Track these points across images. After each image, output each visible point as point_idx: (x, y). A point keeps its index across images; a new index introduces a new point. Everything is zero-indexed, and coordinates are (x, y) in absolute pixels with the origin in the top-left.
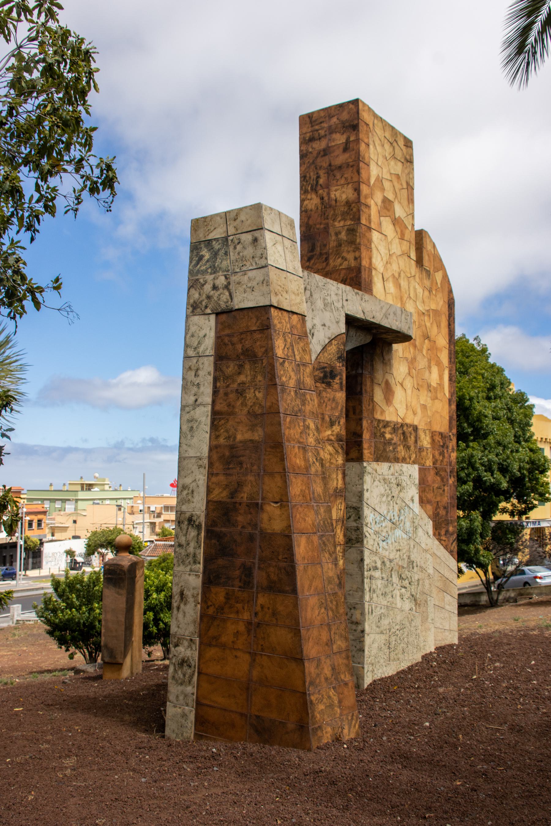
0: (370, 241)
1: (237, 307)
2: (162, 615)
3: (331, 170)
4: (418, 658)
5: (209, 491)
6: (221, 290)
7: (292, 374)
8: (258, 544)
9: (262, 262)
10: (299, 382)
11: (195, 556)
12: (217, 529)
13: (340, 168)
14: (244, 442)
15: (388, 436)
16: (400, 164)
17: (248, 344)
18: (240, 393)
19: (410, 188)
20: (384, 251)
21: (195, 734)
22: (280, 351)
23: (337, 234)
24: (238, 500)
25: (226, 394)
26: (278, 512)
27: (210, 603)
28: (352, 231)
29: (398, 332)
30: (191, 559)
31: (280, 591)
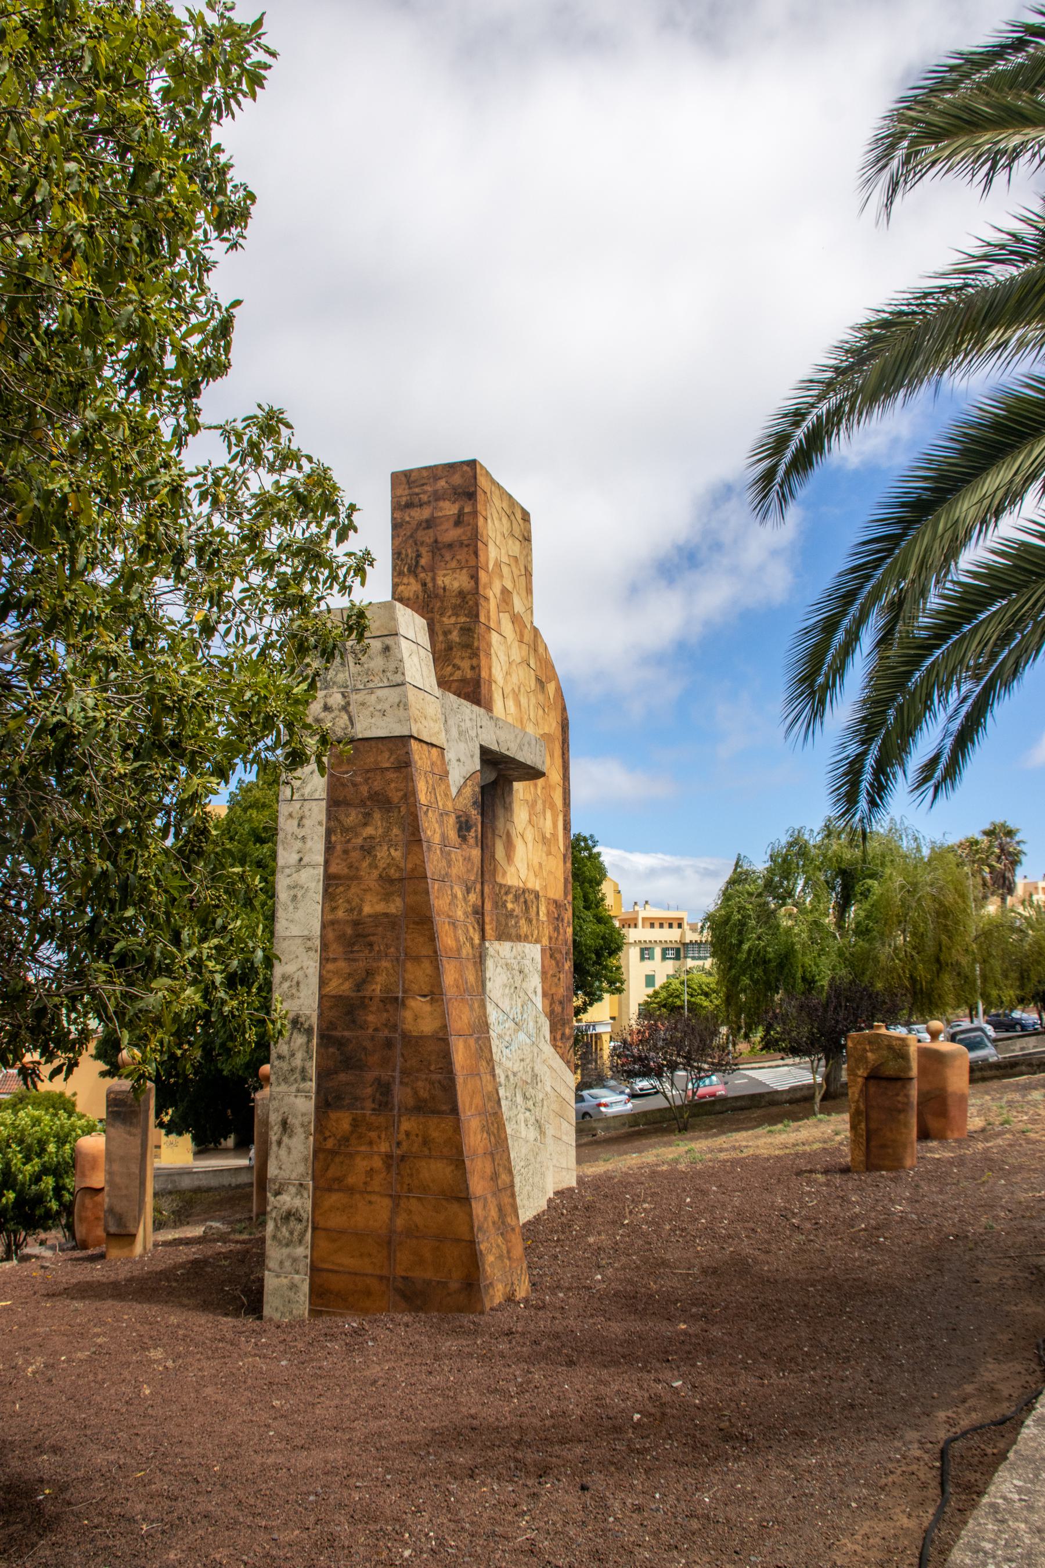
0: (489, 645)
1: (360, 736)
2: (67, 1181)
3: (437, 548)
4: (543, 1205)
5: (323, 982)
6: (336, 713)
7: (436, 826)
8: (398, 1052)
9: (398, 678)
10: (444, 837)
11: (303, 1070)
12: (337, 1034)
13: (450, 546)
14: (375, 916)
15: (510, 906)
16: (518, 543)
17: (377, 785)
18: (368, 850)
19: (528, 574)
20: (503, 660)
21: (310, 1311)
22: (423, 798)
23: (446, 633)
24: (367, 994)
25: (346, 852)
26: (427, 1008)
27: (327, 1134)
28: (467, 631)
29: (532, 768)
30: (297, 1075)
31: (433, 1112)
